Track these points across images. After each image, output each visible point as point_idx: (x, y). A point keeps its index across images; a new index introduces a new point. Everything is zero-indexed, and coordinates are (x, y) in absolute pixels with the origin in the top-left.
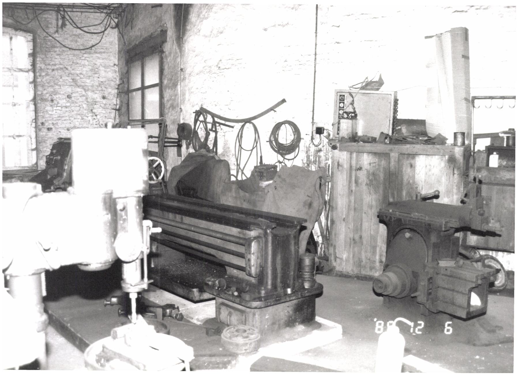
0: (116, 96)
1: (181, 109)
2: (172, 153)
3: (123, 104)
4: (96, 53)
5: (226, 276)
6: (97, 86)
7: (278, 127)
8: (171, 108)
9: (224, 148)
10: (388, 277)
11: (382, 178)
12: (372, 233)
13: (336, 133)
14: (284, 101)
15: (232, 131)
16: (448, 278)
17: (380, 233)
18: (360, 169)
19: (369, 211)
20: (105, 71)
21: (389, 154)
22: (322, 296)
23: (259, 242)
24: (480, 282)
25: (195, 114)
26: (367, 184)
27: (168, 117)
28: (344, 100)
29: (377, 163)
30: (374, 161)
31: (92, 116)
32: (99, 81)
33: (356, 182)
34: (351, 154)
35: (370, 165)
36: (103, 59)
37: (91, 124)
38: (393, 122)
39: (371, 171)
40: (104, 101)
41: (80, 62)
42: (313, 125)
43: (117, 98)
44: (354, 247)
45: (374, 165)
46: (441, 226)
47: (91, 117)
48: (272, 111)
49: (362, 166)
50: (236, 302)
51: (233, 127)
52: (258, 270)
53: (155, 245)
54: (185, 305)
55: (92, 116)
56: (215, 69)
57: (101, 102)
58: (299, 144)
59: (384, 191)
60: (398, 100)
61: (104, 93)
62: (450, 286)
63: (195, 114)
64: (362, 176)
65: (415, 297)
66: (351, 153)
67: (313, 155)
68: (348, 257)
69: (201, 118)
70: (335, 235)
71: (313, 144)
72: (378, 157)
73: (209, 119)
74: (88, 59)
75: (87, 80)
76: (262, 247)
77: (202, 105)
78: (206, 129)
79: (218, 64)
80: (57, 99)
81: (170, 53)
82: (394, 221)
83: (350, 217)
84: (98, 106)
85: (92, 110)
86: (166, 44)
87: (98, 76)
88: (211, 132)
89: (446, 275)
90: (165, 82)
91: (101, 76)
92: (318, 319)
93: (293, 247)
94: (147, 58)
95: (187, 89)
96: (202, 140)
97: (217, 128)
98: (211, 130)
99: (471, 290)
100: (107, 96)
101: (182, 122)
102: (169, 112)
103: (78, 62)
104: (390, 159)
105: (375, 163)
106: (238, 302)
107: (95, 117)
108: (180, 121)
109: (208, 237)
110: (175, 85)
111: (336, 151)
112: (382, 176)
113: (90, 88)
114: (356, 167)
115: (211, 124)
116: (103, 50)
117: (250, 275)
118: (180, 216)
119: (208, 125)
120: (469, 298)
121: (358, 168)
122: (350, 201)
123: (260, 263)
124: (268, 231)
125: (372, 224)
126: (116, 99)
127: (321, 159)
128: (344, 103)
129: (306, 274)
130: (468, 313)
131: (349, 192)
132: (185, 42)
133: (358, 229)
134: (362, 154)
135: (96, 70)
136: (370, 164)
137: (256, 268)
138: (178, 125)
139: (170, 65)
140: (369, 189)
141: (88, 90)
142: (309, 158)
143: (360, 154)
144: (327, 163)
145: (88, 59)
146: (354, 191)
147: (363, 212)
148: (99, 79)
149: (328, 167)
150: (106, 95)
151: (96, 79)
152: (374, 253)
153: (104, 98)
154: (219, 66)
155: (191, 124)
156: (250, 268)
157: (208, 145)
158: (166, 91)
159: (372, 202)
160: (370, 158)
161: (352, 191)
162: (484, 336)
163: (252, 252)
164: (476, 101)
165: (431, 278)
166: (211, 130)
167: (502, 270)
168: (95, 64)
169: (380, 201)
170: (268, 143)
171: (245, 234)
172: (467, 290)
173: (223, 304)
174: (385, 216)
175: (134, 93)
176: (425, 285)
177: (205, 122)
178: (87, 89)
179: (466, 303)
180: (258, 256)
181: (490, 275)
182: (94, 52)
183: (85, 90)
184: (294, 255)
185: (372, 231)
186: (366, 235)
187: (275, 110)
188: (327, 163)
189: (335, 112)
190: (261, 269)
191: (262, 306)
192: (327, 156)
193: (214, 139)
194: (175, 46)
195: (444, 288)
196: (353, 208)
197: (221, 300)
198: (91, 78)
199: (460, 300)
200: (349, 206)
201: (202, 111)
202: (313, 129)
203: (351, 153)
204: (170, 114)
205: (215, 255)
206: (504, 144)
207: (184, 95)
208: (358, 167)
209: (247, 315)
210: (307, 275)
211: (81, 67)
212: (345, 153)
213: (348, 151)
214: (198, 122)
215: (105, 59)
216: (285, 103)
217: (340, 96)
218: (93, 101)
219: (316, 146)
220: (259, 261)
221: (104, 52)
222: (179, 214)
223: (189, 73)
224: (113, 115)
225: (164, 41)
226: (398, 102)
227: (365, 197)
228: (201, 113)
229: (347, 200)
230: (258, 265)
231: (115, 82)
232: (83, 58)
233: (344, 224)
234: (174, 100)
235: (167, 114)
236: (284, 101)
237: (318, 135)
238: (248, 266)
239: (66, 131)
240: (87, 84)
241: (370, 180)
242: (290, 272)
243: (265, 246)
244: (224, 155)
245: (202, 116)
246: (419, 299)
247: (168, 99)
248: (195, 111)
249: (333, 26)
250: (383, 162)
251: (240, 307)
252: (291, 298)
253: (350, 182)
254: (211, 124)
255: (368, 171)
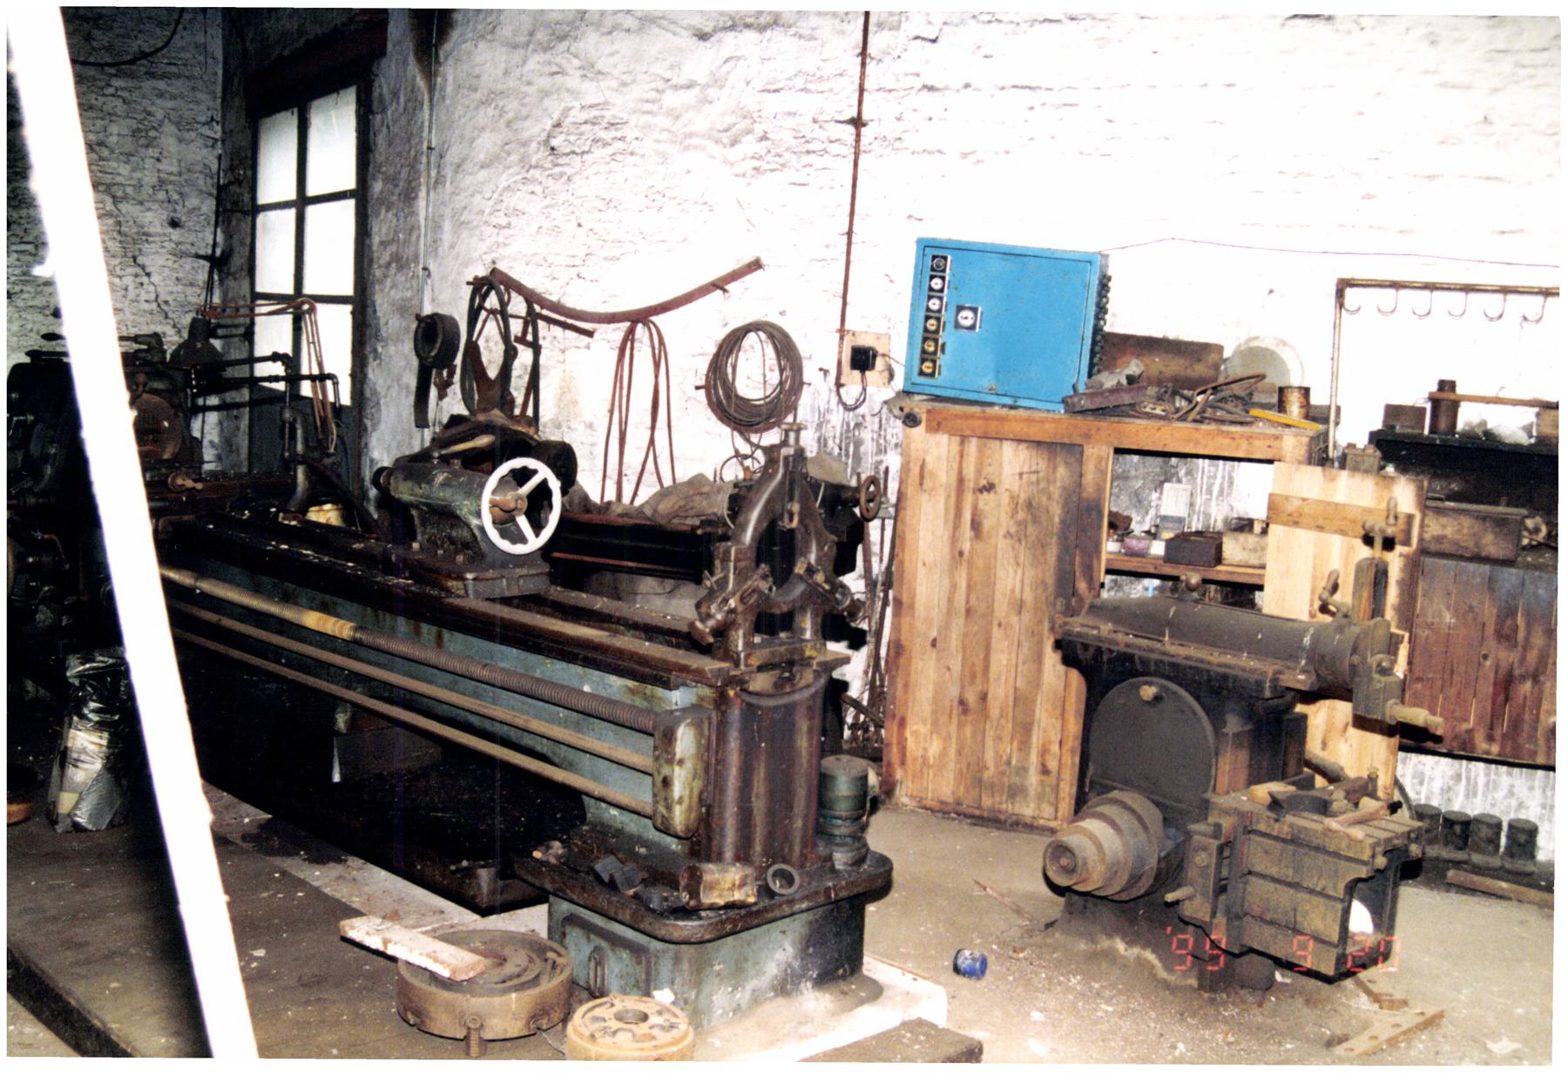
0: (213, 222)
1: (425, 269)
2: (392, 410)
3: (1048, 789)
4: (152, 75)
5: (585, 828)
6: (154, 187)
7: (732, 343)
8: (394, 265)
9: (560, 400)
10: (1086, 832)
11: (1057, 519)
12: (1018, 684)
13: (916, 370)
14: (756, 265)
15: (588, 347)
16: (1279, 845)
17: (1045, 687)
18: (990, 488)
19: (1014, 619)
20: (180, 140)
21: (1082, 446)
22: (894, 895)
23: (697, 725)
24: (1381, 862)
25: (471, 287)
26: (1008, 534)
27: (382, 290)
28: (944, 271)
29: (1041, 474)
30: (1034, 468)
31: (136, 276)
32: (159, 171)
33: (976, 526)
34: (962, 443)
35: (1021, 478)
36: (173, 97)
37: (132, 301)
38: (1094, 343)
39: (1023, 497)
40: (176, 234)
41: (99, 103)
42: (842, 338)
43: (216, 226)
44: (961, 725)
45: (1034, 477)
46: (1259, 684)
47: (131, 278)
48: (719, 292)
49: (996, 482)
50: (620, 917)
51: (590, 334)
52: (693, 815)
53: (344, 712)
54: (442, 912)
55: (136, 276)
56: (538, 155)
57: (164, 235)
58: (797, 399)
59: (1060, 559)
60: (1109, 279)
61: (175, 211)
62: (1289, 874)
63: (471, 287)
64: (998, 512)
65: (1177, 903)
66: (964, 439)
67: (838, 434)
68: (944, 753)
69: (492, 301)
70: (906, 686)
71: (841, 401)
72: (1046, 457)
73: (518, 306)
74: (125, 94)
75: (122, 165)
76: (709, 739)
77: (494, 262)
78: (505, 336)
79: (549, 136)
80: (23, 221)
81: (395, 95)
82: (1110, 661)
83: (954, 637)
84: (153, 245)
85: (135, 258)
86: (384, 62)
87: (156, 155)
88: (520, 347)
89: (1276, 838)
90: (377, 187)
91: (165, 154)
92: (872, 966)
93: (805, 740)
94: (316, 103)
95: (447, 212)
96: (492, 373)
97: (541, 333)
98: (522, 340)
99: (1352, 889)
100: (184, 219)
101: (428, 310)
102: (386, 277)
103: (94, 102)
104: (1081, 462)
105: (1037, 472)
106: (627, 917)
107: (145, 280)
108: (421, 308)
109: (524, 698)
110: (409, 196)
111: (919, 432)
112: (1056, 511)
113: (129, 190)
114: (977, 481)
115: (521, 321)
116: (174, 69)
117: (666, 829)
118: (434, 629)
119: (512, 321)
120: (1346, 912)
121: (984, 487)
122: (954, 587)
123: (701, 793)
124: (731, 693)
125: (1020, 661)
126: (212, 229)
127: (862, 449)
128: (943, 278)
129: (839, 822)
130: (1341, 959)
131: (953, 557)
132: (446, 58)
133: (977, 670)
134: (998, 442)
135: (152, 133)
136: (1021, 475)
137: (690, 809)
138: (419, 318)
139: (395, 129)
140: (1013, 548)
141: (125, 198)
142: (825, 445)
143: (994, 444)
144: (881, 462)
145: (125, 94)
146: (966, 554)
147: (995, 623)
148: (158, 165)
149: (882, 475)
150: (181, 215)
151: (149, 163)
152: (1025, 745)
153: (174, 224)
154: (554, 143)
155: (457, 317)
156: (669, 808)
157: (510, 394)
158: (378, 215)
159: (1022, 591)
160: (1022, 458)
161: (961, 554)
162: (1384, 1023)
163: (678, 757)
164: (1349, 292)
165: (1228, 843)
166: (522, 340)
167: (1405, 806)
168: (150, 114)
169: (1045, 589)
170: (702, 392)
171: (653, 696)
172: (1341, 887)
173: (571, 920)
174: (1082, 644)
175: (272, 215)
176: (1207, 867)
177: (503, 314)
178: (120, 194)
179: (1337, 928)
180: (695, 770)
181: (1409, 837)
182: (146, 73)
183: (114, 197)
184: (805, 765)
185: (1019, 679)
186: (1000, 693)
187: (727, 287)
188: (881, 462)
189: (914, 307)
190: (704, 810)
191: (707, 937)
192: (882, 441)
193: (529, 369)
194: (413, 69)
195: (1263, 876)
196: (963, 610)
197: (565, 907)
198: (132, 159)
199: (1319, 918)
200: (950, 601)
201: (495, 281)
202: (840, 353)
203: (964, 439)
204: (388, 282)
205: (550, 754)
206: (1423, 428)
207: (437, 227)
208: (983, 482)
209: (653, 960)
210: (842, 829)
211: (102, 119)
212: (943, 438)
213: (952, 433)
214: (483, 314)
215: (182, 96)
216: (760, 272)
217: (934, 257)
218: (138, 233)
219: (847, 408)
220: (698, 784)
221: (178, 76)
222: (431, 621)
223: (456, 161)
224: (202, 276)
225: (380, 51)
226: (1110, 284)
227: (1001, 573)
228: (492, 287)
229: (946, 583)
230: (695, 799)
231: (1387, 524)
232: (111, 90)
233: (934, 654)
234: (406, 242)
235: (381, 282)
236: (756, 265)
237: (857, 373)
238: (662, 803)
239: (51, 318)
240: (119, 179)
241: (1019, 524)
242: (790, 818)
243: (718, 740)
244: (559, 426)
245: (493, 294)
246: (1188, 910)
247: (384, 239)
248: (471, 280)
249: (917, 38)
250: (1062, 471)
251: (630, 934)
252: (797, 907)
253: (957, 525)
254: (521, 321)
255: (1014, 499)
